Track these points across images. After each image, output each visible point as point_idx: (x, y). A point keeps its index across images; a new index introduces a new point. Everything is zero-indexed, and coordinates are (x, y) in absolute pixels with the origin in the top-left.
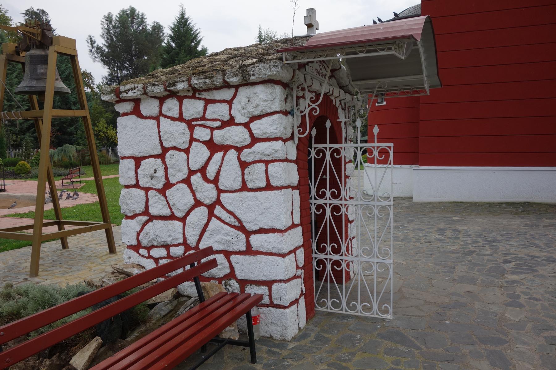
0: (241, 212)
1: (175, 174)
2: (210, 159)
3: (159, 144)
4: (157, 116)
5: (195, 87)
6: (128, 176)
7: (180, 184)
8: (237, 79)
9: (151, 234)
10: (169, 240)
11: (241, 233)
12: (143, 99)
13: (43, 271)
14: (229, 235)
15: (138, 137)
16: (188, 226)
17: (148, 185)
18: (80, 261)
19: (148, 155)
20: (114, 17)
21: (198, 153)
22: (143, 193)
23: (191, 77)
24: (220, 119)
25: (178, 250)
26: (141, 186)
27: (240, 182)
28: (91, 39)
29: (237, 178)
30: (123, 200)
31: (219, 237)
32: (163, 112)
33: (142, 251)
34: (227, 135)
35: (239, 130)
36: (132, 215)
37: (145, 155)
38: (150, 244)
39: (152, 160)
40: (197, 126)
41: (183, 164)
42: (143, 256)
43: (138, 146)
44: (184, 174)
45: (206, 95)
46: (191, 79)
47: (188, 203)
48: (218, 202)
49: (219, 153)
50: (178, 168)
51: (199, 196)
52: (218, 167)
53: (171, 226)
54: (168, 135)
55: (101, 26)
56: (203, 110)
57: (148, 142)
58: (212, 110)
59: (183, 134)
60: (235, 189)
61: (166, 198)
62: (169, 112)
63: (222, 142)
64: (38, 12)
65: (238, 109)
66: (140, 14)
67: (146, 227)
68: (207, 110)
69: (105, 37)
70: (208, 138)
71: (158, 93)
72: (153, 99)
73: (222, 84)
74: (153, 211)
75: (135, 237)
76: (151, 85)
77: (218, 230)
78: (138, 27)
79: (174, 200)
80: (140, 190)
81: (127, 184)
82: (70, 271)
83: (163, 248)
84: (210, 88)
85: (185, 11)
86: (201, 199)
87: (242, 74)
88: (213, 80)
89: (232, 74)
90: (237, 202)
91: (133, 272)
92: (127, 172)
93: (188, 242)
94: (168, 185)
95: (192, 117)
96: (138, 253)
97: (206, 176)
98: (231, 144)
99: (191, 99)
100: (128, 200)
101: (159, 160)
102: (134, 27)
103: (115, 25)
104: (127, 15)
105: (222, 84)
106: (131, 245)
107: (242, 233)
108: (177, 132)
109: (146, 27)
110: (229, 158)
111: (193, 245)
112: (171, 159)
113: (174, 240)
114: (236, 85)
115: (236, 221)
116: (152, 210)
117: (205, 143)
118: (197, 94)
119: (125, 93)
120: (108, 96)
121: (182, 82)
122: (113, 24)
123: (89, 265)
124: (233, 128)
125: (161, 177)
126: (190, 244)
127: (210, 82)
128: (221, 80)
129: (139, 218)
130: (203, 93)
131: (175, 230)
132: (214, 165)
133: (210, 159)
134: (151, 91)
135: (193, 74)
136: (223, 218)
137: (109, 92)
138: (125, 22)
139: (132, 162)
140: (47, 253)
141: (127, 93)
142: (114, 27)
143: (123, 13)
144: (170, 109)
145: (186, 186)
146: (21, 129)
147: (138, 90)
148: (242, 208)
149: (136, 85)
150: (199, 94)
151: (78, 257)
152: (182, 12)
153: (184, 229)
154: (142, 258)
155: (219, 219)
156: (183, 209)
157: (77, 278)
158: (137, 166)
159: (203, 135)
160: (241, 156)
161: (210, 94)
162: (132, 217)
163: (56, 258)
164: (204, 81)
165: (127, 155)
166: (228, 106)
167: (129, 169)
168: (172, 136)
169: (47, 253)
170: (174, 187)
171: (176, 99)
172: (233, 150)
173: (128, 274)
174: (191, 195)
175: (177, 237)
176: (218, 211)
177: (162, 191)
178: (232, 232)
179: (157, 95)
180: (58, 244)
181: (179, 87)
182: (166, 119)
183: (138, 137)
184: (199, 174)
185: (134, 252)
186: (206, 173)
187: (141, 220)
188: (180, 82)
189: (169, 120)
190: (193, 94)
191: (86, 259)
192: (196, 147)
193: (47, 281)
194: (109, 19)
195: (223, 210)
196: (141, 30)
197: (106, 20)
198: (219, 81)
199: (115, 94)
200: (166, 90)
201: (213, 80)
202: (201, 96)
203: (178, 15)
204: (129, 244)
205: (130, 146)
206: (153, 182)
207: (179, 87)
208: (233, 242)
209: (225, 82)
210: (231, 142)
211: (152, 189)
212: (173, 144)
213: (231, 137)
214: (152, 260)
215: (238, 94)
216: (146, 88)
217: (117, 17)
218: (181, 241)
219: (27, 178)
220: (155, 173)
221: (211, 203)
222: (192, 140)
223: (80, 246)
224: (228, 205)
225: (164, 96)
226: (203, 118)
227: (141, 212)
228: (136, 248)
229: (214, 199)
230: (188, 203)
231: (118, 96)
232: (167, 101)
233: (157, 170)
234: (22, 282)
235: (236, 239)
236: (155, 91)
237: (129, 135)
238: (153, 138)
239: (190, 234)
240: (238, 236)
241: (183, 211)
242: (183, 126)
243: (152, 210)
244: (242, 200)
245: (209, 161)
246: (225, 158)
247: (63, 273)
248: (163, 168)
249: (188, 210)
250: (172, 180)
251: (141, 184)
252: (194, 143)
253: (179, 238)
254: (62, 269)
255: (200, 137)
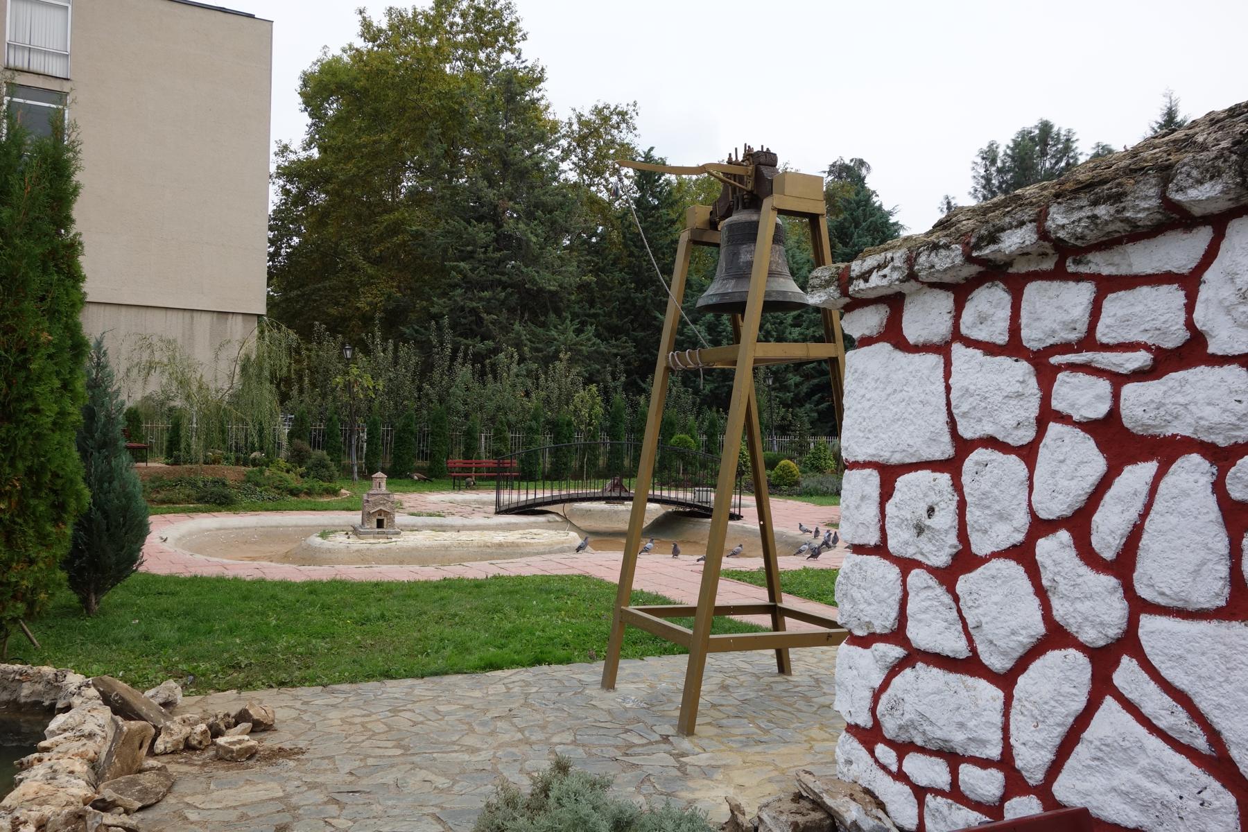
0: (1223, 702)
1: (987, 526)
2: (1104, 484)
3: (946, 429)
4: (947, 342)
5: (1058, 238)
6: (861, 518)
7: (1002, 560)
8: (1219, 188)
9: (908, 707)
10: (958, 739)
11: (1217, 785)
12: (910, 295)
13: (710, 724)
14: (1167, 782)
15: (891, 407)
16: (1019, 707)
17: (910, 552)
18: (799, 715)
19: (914, 460)
20: (1001, 152)
21: (1062, 462)
22: (893, 572)
23: (1048, 207)
24: (1150, 342)
25: (983, 779)
26: (891, 551)
27: (1221, 583)
28: (949, 203)
29: (1210, 565)
30: (845, 587)
31: (1126, 776)
32: (964, 330)
33: (881, 749)
34: (1175, 400)
35: (1222, 380)
36: (865, 634)
37: (908, 461)
38: (904, 737)
39: (925, 475)
40: (1066, 369)
41: (1015, 496)
42: (884, 768)
43: (890, 434)
44: (1017, 530)
45: (1102, 264)
46: (1047, 214)
47: (1024, 628)
48: (1128, 643)
49: (1141, 465)
50: (997, 507)
51: (1061, 612)
52: (1133, 514)
53: (966, 694)
54: (971, 399)
55: (973, 173)
56: (1087, 315)
57: (914, 420)
58: (1120, 313)
59: (1019, 395)
60: (1198, 607)
61: (956, 599)
62: (980, 327)
63: (1154, 426)
64: (852, 164)
65: (1220, 302)
66: (1063, 132)
67: (897, 681)
68: (1103, 315)
69: (980, 195)
70: (1100, 410)
71: (945, 270)
72: (937, 291)
73: (1159, 216)
74: (919, 635)
75: (867, 703)
76: (927, 249)
77: (1125, 750)
78: (1057, 163)
79: (980, 611)
80: (887, 562)
81: (856, 542)
82: (764, 738)
83: (940, 761)
84: (1117, 235)
85: (1176, 105)
86: (1068, 624)
87: (1240, 167)
88: (1123, 205)
89: (1195, 173)
90: (1204, 659)
91: (846, 815)
92: (857, 507)
93: (1019, 764)
94: (965, 560)
95: (1050, 341)
96: (872, 752)
97: (1090, 544)
98: (1188, 432)
99: (1049, 282)
100: (855, 588)
101: (944, 479)
102: (1048, 165)
103: (1004, 167)
104: (1032, 139)
105: (1159, 216)
106: (857, 726)
107: (1224, 786)
108: (999, 389)
109: (1076, 159)
110: (1176, 487)
111: (1035, 777)
112: (977, 478)
113: (973, 744)
114: (1216, 211)
115: (1197, 730)
116: (916, 631)
117: (1089, 426)
118: (1069, 262)
119: (861, 281)
120: (822, 294)
121: (1016, 227)
122: (999, 164)
123: (815, 732)
124: (1200, 376)
125: (947, 532)
126: (1024, 773)
127: (1112, 212)
128: (1154, 202)
129: (880, 647)
130: (1090, 257)
131: (976, 710)
132: (1119, 508)
133: (1104, 484)
134: (927, 265)
135: (1057, 196)
136: (1147, 710)
137: (826, 281)
138: (1027, 157)
139: (873, 477)
140: (742, 678)
141: (866, 281)
142: (999, 171)
143: (1023, 137)
144: (982, 319)
145: (1021, 569)
146: (796, 395)
147: (894, 269)
148: (1225, 685)
149: (889, 255)
150: (1077, 262)
151: (801, 704)
152: (1170, 109)
153: (1006, 714)
154: (881, 773)
155: (1131, 707)
156: (1005, 646)
157: (768, 764)
158: (886, 492)
159: (1083, 401)
160: (1228, 481)
161: (1117, 259)
162: (865, 642)
163: (752, 695)
164: (1089, 214)
165: (861, 459)
166: (1182, 293)
167: (863, 498)
168: (983, 404)
169: (742, 678)
170: (980, 569)
171: (1001, 285)
172: (1195, 458)
173: (831, 814)
174: (1036, 602)
175: (983, 737)
176: (1127, 674)
177: (947, 576)
178: (1182, 770)
179: (947, 279)
180: (768, 657)
181: (1007, 244)
182: (971, 351)
183: (891, 407)
184: (1064, 536)
185: (860, 747)
186: (1090, 534)
187: (884, 655)
188: (1010, 229)
189: (978, 353)
190: (1056, 264)
191: (815, 713)
192: (1059, 443)
193: (705, 756)
194: (990, 156)
195: (1146, 676)
196: (1062, 168)
197: (983, 158)
198: (1144, 205)
199: (838, 286)
200: (969, 259)
201: (1123, 205)
202: (1083, 269)
203: (1158, 117)
204: (852, 721)
205: (870, 431)
206: (921, 545)
207: (1007, 244)
208: (1183, 814)
209: (1168, 205)
210: (1190, 425)
211: (918, 564)
212: (986, 428)
213: (1191, 407)
214: (907, 789)
215: (1224, 245)
216: (915, 260)
217: (1008, 147)
218: (994, 752)
219: (790, 495)
220: (929, 516)
221: (1102, 643)
222: (1047, 415)
223: (817, 674)
224: (1169, 664)
225: (966, 279)
226: (1089, 342)
227: (886, 631)
228: (869, 736)
229: (1114, 632)
230: (1024, 628)
231: (845, 293)
232: (975, 294)
233: (937, 509)
234: (657, 742)
235: (1195, 805)
236: (937, 267)
237: (869, 400)
238: (929, 409)
239: (1025, 737)
240: (1204, 795)
241: (1004, 654)
242: (1021, 372)
243: (916, 631)
244: (1228, 653)
245: (1104, 492)
246: (1162, 486)
247: (748, 741)
248: (955, 504)
249: (1021, 651)
250: (980, 546)
251: (893, 545)
252: (1054, 428)
253: (988, 741)
254: (751, 728)
255: (1072, 406)
